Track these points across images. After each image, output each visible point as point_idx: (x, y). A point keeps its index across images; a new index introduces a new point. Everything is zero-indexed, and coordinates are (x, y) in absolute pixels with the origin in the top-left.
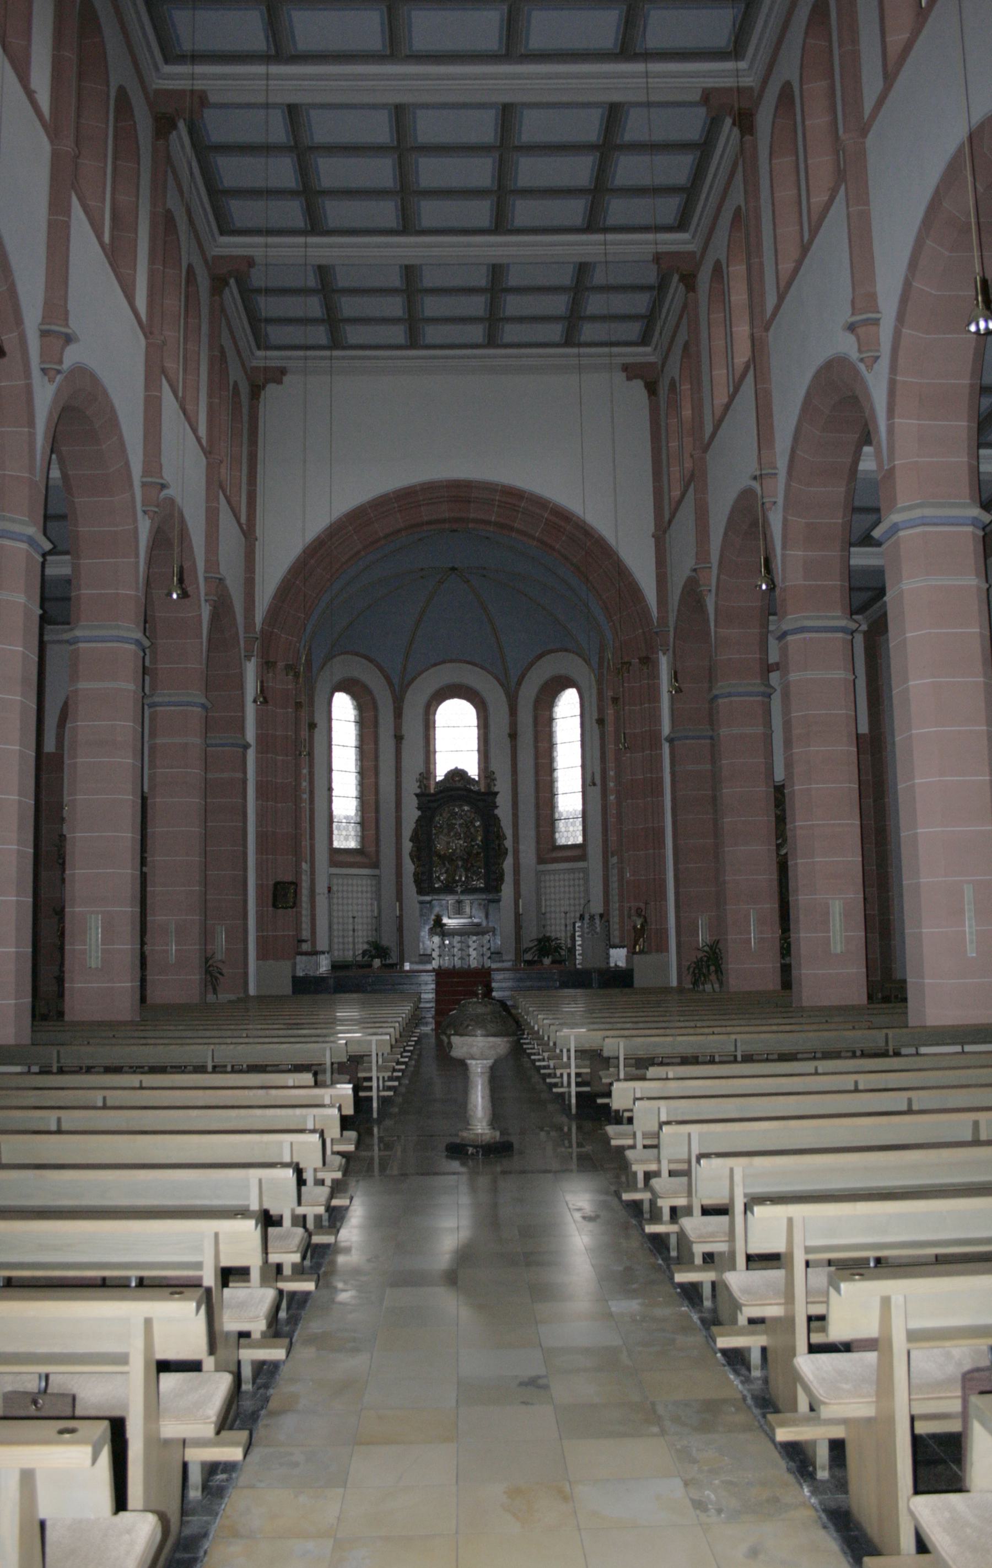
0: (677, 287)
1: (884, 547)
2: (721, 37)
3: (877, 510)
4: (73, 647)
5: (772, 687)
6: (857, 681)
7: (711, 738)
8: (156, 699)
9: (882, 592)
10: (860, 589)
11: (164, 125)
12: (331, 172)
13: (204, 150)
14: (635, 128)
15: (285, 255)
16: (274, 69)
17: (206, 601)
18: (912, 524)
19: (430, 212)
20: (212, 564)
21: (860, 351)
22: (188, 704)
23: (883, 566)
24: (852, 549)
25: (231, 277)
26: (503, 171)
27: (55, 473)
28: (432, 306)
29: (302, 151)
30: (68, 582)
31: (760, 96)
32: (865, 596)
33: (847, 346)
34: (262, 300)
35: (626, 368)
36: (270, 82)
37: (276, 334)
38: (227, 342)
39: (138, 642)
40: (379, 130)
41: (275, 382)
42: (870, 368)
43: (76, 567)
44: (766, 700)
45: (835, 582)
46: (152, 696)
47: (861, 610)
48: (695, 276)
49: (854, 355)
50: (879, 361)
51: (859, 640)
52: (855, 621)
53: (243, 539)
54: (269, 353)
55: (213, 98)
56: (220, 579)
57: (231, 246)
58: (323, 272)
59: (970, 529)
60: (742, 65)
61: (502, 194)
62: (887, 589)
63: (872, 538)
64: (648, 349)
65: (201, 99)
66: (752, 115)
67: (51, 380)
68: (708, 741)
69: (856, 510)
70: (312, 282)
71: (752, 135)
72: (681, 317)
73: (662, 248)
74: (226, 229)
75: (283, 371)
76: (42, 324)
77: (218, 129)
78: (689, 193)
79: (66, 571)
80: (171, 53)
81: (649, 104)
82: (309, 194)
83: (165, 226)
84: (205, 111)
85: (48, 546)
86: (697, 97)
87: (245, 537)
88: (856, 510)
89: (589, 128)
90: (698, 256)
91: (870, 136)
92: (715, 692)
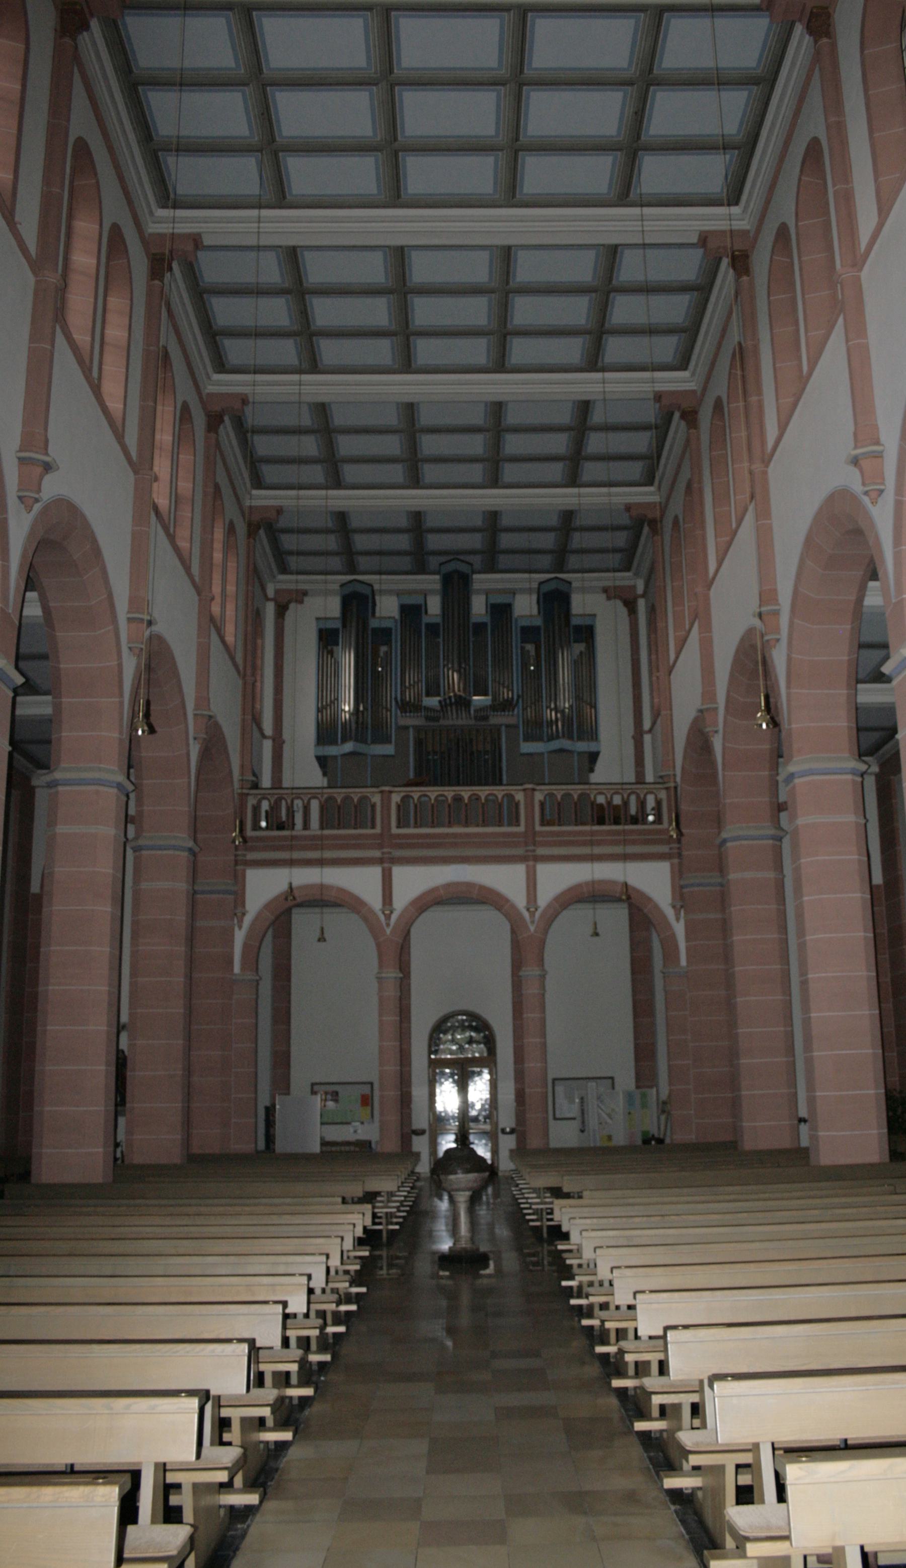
0: (678, 425)
1: (894, 683)
2: (716, 185)
3: (885, 646)
4: (53, 790)
5: (782, 829)
6: (869, 825)
7: (721, 885)
8: (141, 842)
9: (894, 730)
10: (867, 729)
11: (159, 266)
12: (325, 313)
13: (200, 294)
14: (630, 269)
15: (278, 391)
16: (306, 377)
17: (195, 739)
18: (804, 774)
19: (425, 350)
20: (203, 700)
21: (864, 484)
22: (175, 848)
23: (894, 703)
24: (860, 686)
25: (226, 419)
26: (504, 310)
27: (33, 610)
28: (430, 445)
29: (298, 291)
30: (48, 722)
31: (756, 239)
32: (875, 736)
33: (853, 481)
34: (160, 102)
35: (605, 590)
36: (302, 387)
37: (187, 174)
38: (222, 478)
39: (119, 786)
40: (374, 270)
41: (296, 601)
42: (874, 502)
43: (57, 707)
44: (778, 843)
45: (841, 723)
46: (136, 838)
47: (871, 752)
48: (696, 412)
49: (857, 487)
50: (884, 494)
51: (870, 783)
52: (865, 762)
53: (196, 598)
54: (180, 213)
55: (207, 241)
56: (210, 717)
57: (262, 498)
58: (322, 409)
59: (849, 777)
60: (735, 210)
61: (502, 334)
62: (899, 729)
63: (883, 675)
64: (685, 374)
65: (196, 241)
66: (747, 257)
67: (29, 509)
68: (718, 888)
69: (862, 646)
70: (306, 421)
71: (695, 429)
72: (684, 452)
73: (659, 387)
74: (221, 366)
75: (305, 593)
76: (20, 451)
77: (212, 271)
78: (690, 331)
79: (48, 711)
80: (167, 197)
81: (644, 246)
82: (307, 334)
83: (158, 364)
84: (200, 254)
85: (20, 680)
86: (695, 240)
87: (199, 593)
88: (862, 646)
89: (583, 269)
90: (751, 235)
91: (772, 464)
92: (724, 835)
